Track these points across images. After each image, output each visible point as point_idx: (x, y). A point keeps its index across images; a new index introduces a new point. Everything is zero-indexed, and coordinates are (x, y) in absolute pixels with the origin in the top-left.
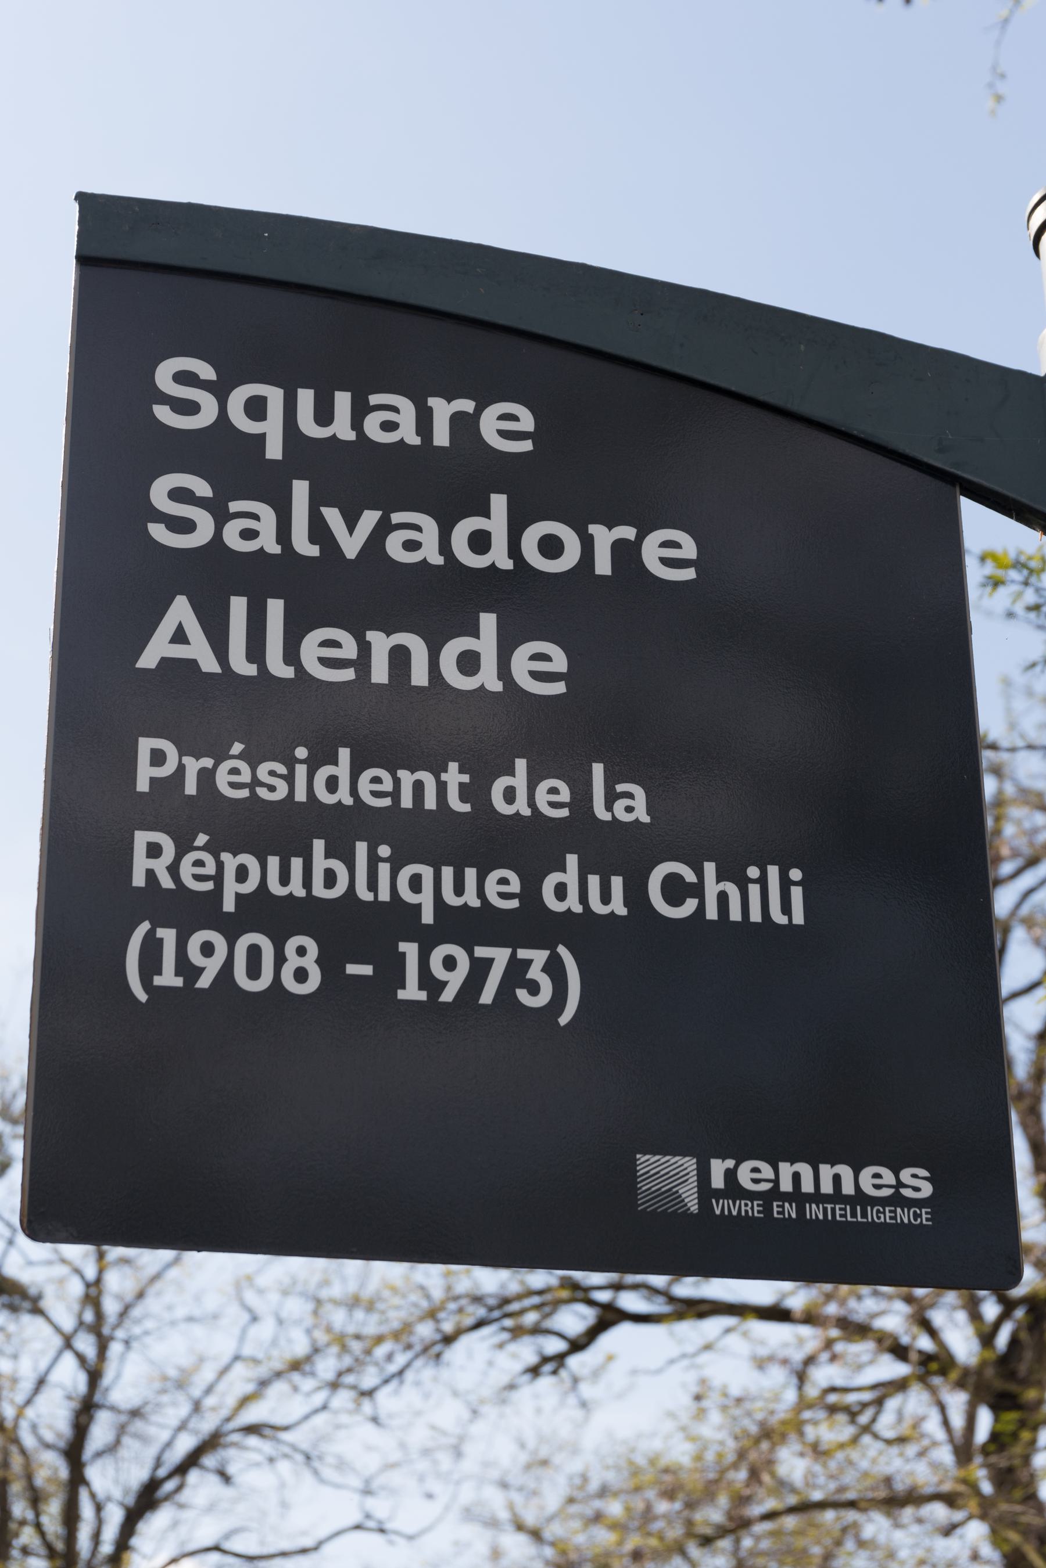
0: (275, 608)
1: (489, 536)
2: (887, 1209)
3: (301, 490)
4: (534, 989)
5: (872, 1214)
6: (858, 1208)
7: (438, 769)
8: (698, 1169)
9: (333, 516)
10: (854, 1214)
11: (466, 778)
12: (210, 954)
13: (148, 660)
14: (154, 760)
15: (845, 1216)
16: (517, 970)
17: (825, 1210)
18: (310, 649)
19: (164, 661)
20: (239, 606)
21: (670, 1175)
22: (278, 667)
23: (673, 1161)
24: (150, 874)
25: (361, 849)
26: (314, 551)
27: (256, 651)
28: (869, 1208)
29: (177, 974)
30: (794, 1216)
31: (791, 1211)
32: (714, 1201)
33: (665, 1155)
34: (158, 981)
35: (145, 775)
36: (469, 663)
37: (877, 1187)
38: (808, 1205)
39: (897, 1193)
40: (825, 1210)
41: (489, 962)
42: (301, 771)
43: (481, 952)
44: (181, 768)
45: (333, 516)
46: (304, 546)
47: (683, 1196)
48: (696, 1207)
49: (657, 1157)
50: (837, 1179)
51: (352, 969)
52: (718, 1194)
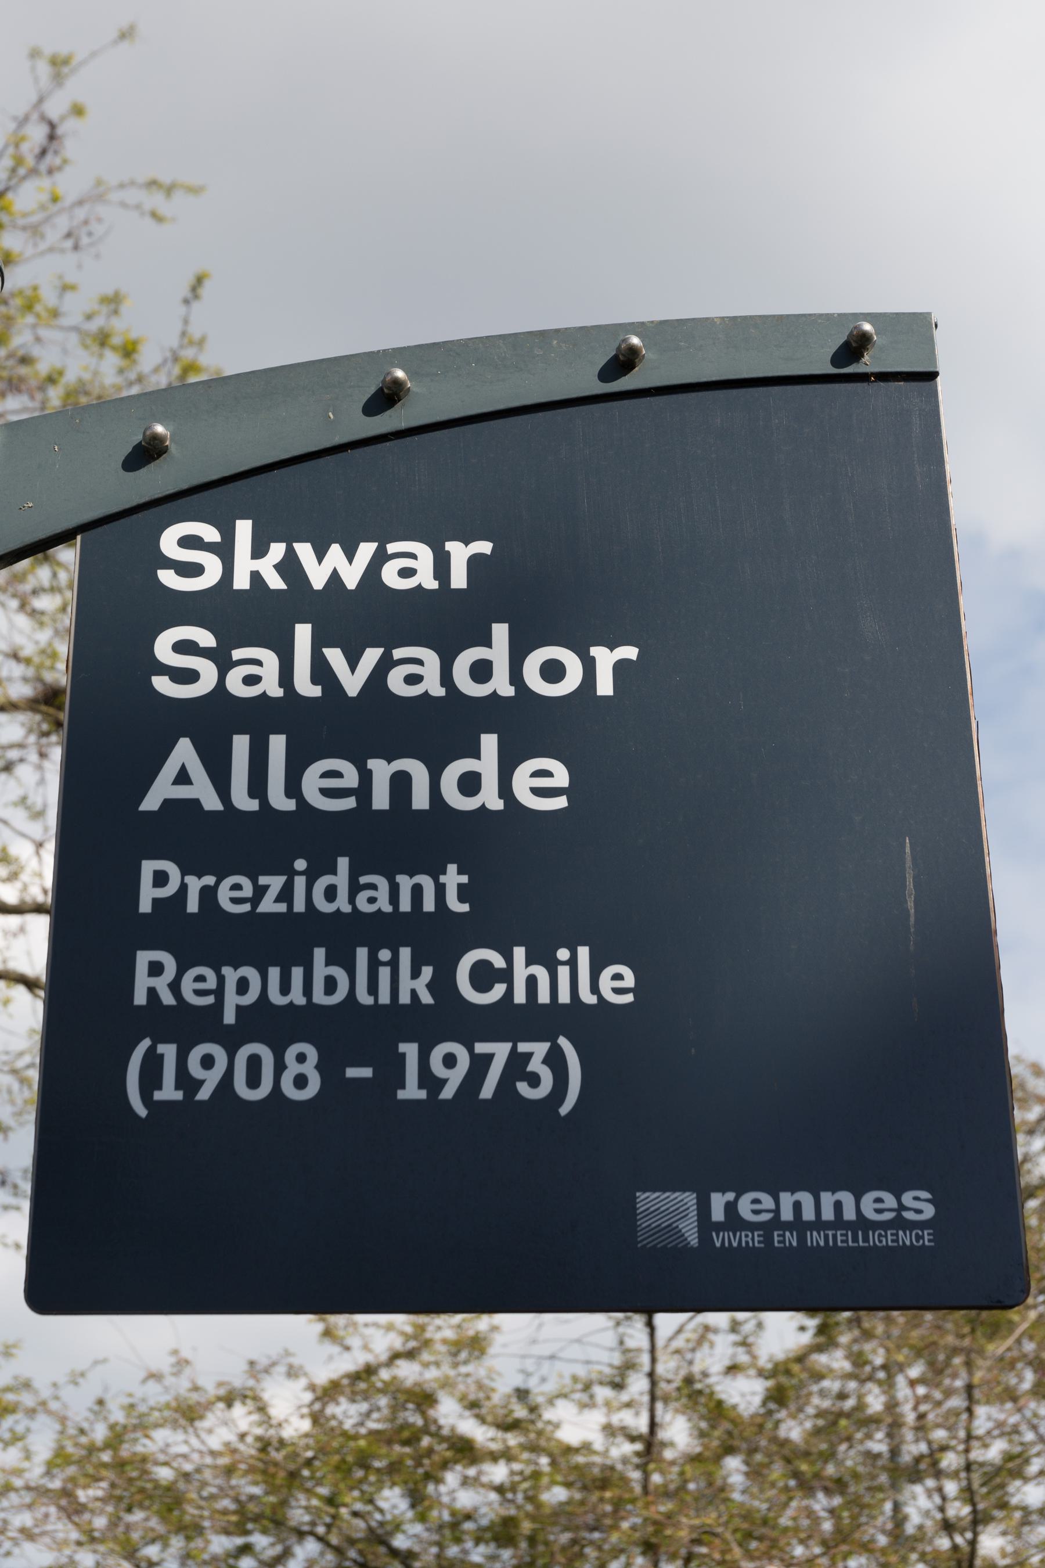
0: (278, 744)
1: (493, 665)
2: (889, 1233)
3: (303, 633)
4: (534, 1080)
5: (874, 1238)
6: (860, 1233)
7: (436, 872)
8: (698, 1204)
9: (335, 656)
10: (855, 1239)
11: (464, 879)
12: (210, 1066)
13: (151, 803)
14: (157, 881)
15: (847, 1241)
16: (517, 1064)
17: (826, 1237)
18: (312, 781)
19: (167, 803)
20: (241, 744)
21: (670, 1211)
22: (280, 800)
23: (672, 1197)
24: (152, 992)
25: (362, 954)
26: (316, 691)
27: (258, 786)
28: (871, 1233)
29: (177, 1088)
30: (795, 1244)
31: (792, 1239)
32: (714, 1234)
33: (664, 1192)
34: (158, 1096)
35: (147, 896)
36: (470, 784)
37: (879, 1211)
38: (809, 1233)
39: (899, 1216)
40: (826, 1237)
41: (489, 1058)
42: (300, 882)
43: (481, 1048)
44: (183, 888)
45: (335, 656)
46: (305, 686)
47: (686, 1235)
48: (696, 1240)
49: (657, 1194)
50: (838, 1206)
51: (352, 1072)
52: (719, 1227)
